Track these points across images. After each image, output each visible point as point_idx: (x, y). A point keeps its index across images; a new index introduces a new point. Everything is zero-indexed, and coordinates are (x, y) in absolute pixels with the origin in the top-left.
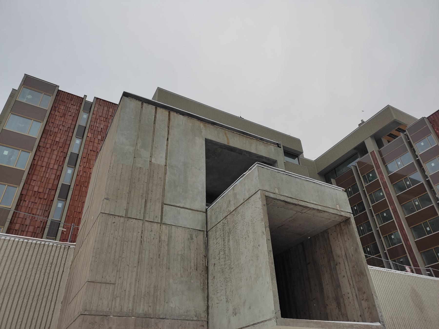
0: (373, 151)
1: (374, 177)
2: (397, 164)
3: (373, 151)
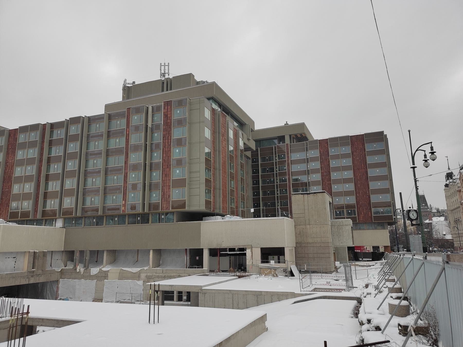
0: (288, 144)
1: (284, 158)
2: (297, 156)
3: (288, 144)
